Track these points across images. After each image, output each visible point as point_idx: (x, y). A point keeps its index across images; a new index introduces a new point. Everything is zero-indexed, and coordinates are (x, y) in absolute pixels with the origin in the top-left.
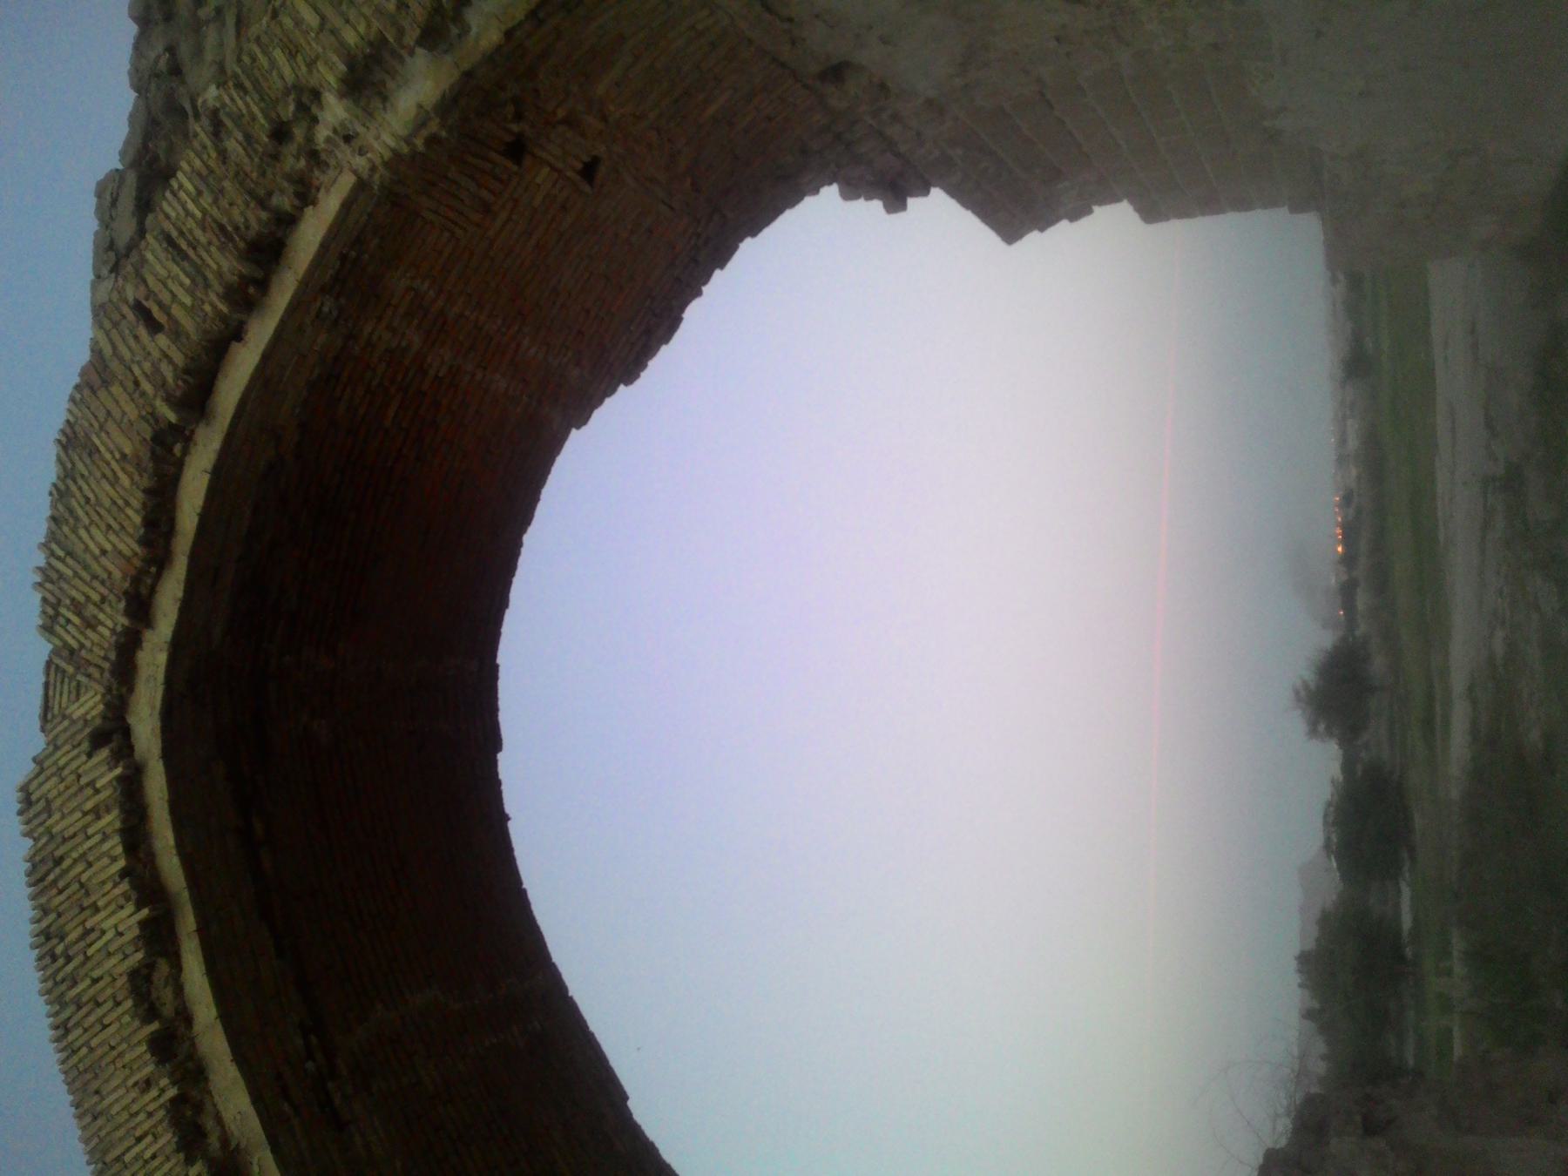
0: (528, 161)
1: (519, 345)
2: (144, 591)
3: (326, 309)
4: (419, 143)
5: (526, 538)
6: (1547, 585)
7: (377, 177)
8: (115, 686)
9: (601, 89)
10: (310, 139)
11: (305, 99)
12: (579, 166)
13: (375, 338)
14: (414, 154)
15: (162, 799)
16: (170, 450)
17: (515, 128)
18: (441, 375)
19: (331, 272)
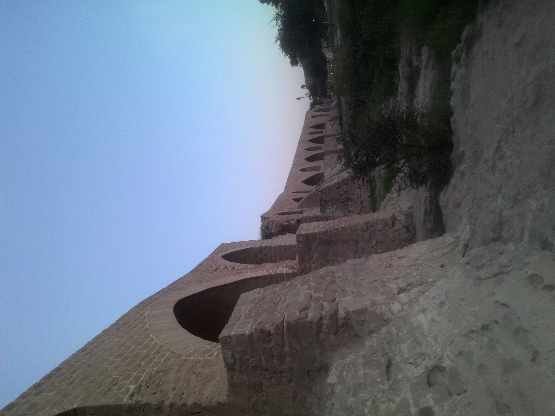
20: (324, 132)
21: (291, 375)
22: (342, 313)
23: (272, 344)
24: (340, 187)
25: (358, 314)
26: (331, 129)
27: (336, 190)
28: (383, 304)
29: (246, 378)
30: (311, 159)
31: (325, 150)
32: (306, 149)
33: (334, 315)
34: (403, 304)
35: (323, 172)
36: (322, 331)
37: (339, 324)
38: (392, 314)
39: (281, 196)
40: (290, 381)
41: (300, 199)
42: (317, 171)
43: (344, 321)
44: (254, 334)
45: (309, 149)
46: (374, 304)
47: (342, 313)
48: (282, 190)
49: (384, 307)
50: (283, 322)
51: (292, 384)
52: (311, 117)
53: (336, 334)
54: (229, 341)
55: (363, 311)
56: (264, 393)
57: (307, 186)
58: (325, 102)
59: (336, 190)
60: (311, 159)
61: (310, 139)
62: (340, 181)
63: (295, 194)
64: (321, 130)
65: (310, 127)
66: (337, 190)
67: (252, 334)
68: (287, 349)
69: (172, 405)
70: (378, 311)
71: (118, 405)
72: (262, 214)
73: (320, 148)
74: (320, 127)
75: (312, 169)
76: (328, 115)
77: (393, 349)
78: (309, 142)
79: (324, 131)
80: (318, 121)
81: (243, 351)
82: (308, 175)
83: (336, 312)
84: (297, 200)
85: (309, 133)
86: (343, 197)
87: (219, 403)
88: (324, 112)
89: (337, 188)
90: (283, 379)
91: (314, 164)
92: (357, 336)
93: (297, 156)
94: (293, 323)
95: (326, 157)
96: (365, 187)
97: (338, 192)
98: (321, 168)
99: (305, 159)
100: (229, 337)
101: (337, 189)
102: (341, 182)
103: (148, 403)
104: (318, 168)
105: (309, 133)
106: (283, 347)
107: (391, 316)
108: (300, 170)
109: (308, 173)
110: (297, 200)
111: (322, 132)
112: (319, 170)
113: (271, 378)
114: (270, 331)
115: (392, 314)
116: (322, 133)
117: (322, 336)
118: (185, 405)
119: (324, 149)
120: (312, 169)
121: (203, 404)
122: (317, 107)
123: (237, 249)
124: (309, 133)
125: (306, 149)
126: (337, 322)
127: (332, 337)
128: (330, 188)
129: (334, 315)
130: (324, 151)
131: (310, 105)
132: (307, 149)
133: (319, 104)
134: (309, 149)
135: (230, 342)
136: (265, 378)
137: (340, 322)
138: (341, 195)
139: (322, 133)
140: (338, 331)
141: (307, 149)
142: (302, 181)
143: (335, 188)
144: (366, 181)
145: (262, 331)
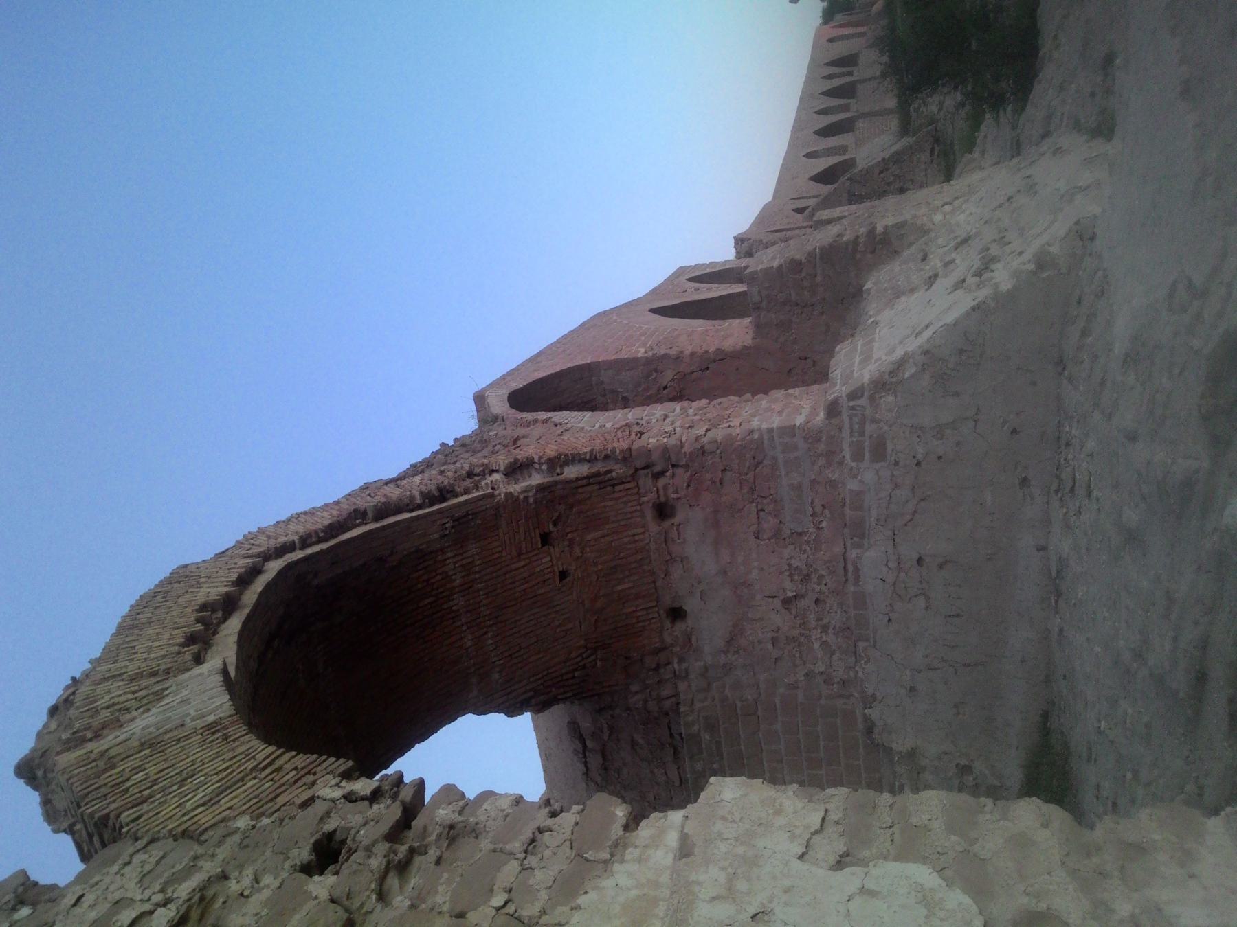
0: (546, 548)
1: (486, 633)
2: (309, 541)
3: (447, 525)
4: (521, 497)
5: (417, 745)
6: (852, 485)
7: (499, 497)
8: (272, 551)
9: (589, 537)
10: (480, 481)
11: (486, 471)
12: (561, 569)
13: (448, 561)
14: (517, 499)
15: (473, 416)
16: (356, 519)
17: (551, 528)
18: (453, 608)
19: (460, 514)
20: (855, 73)
21: (822, 307)
22: (880, 229)
23: (804, 275)
24: (887, 169)
25: (898, 228)
26: (871, 63)
27: (879, 174)
28: (923, 216)
29: (773, 316)
30: (826, 132)
31: (857, 111)
32: (815, 112)
33: (872, 232)
34: (945, 214)
35: (852, 156)
36: (859, 249)
37: (877, 240)
38: (933, 224)
39: (766, 207)
40: (822, 313)
41: (805, 208)
42: (840, 155)
43: (881, 237)
44: (784, 266)
45: (823, 112)
46: (915, 216)
47: (880, 229)
48: (768, 197)
49: (925, 218)
50: (815, 249)
51: (824, 317)
52: (827, 41)
53: (873, 252)
54: (755, 276)
55: (903, 225)
56: (793, 331)
57: (821, 186)
58: (857, 5)
59: (879, 174)
60: (826, 132)
61: (825, 89)
62: (887, 156)
63: (796, 201)
64: (845, 101)
65: (825, 64)
66: (882, 175)
67: (781, 265)
68: (819, 279)
69: (693, 354)
70: (919, 223)
71: (634, 358)
72: (735, 235)
73: (846, 108)
74: (847, 61)
75: (829, 152)
76: (864, 34)
77: (887, 51)
78: (822, 96)
79: (855, 70)
80: (841, 49)
81: (770, 286)
82: (822, 164)
83: (874, 228)
84: (800, 211)
85: (822, 78)
86: (892, 187)
87: (745, 348)
88: (855, 29)
89: (882, 169)
90: (815, 313)
91: (833, 142)
92: (896, 252)
93: (798, 127)
94: (827, 247)
95: (860, 124)
96: (936, 166)
97: (883, 179)
98: (849, 149)
99: (815, 133)
100: (756, 272)
101: (881, 172)
102: (889, 158)
103: (667, 354)
104: (844, 149)
105: (822, 76)
106: (816, 276)
107: (932, 226)
108: (804, 156)
109: (822, 160)
110: (800, 211)
111: (850, 74)
112: (844, 154)
113: (802, 313)
114: (801, 261)
115: (933, 224)
116: (852, 75)
117: (858, 256)
118: (706, 352)
119: (855, 110)
120: (829, 152)
121: (726, 350)
122: (839, 18)
123: (708, 270)
124: (822, 78)
125: (815, 112)
126: (875, 238)
127: (869, 256)
128: (867, 170)
129: (872, 232)
130: (856, 114)
131: (821, 15)
132: (820, 112)
133: (843, 12)
134: (823, 112)
135: (757, 278)
136: (794, 314)
137: (878, 238)
138: (889, 184)
139: (852, 75)
140: (875, 249)
141: (820, 112)
142: (809, 177)
143: (877, 172)
144: (936, 153)
145: (792, 261)
